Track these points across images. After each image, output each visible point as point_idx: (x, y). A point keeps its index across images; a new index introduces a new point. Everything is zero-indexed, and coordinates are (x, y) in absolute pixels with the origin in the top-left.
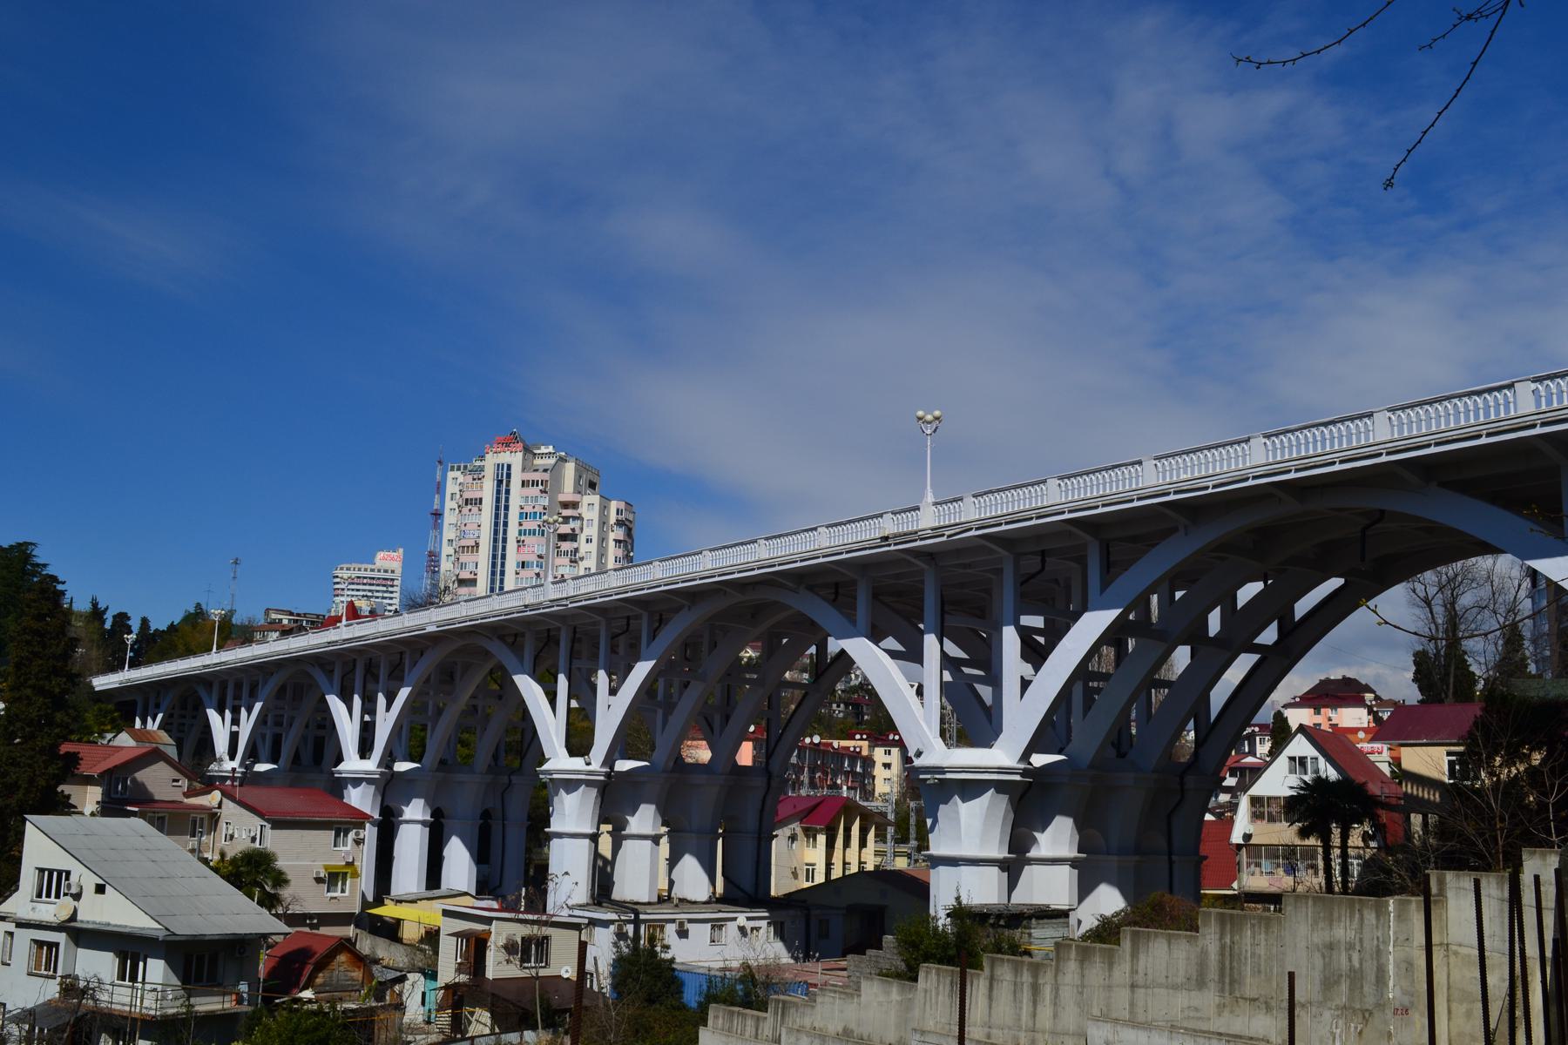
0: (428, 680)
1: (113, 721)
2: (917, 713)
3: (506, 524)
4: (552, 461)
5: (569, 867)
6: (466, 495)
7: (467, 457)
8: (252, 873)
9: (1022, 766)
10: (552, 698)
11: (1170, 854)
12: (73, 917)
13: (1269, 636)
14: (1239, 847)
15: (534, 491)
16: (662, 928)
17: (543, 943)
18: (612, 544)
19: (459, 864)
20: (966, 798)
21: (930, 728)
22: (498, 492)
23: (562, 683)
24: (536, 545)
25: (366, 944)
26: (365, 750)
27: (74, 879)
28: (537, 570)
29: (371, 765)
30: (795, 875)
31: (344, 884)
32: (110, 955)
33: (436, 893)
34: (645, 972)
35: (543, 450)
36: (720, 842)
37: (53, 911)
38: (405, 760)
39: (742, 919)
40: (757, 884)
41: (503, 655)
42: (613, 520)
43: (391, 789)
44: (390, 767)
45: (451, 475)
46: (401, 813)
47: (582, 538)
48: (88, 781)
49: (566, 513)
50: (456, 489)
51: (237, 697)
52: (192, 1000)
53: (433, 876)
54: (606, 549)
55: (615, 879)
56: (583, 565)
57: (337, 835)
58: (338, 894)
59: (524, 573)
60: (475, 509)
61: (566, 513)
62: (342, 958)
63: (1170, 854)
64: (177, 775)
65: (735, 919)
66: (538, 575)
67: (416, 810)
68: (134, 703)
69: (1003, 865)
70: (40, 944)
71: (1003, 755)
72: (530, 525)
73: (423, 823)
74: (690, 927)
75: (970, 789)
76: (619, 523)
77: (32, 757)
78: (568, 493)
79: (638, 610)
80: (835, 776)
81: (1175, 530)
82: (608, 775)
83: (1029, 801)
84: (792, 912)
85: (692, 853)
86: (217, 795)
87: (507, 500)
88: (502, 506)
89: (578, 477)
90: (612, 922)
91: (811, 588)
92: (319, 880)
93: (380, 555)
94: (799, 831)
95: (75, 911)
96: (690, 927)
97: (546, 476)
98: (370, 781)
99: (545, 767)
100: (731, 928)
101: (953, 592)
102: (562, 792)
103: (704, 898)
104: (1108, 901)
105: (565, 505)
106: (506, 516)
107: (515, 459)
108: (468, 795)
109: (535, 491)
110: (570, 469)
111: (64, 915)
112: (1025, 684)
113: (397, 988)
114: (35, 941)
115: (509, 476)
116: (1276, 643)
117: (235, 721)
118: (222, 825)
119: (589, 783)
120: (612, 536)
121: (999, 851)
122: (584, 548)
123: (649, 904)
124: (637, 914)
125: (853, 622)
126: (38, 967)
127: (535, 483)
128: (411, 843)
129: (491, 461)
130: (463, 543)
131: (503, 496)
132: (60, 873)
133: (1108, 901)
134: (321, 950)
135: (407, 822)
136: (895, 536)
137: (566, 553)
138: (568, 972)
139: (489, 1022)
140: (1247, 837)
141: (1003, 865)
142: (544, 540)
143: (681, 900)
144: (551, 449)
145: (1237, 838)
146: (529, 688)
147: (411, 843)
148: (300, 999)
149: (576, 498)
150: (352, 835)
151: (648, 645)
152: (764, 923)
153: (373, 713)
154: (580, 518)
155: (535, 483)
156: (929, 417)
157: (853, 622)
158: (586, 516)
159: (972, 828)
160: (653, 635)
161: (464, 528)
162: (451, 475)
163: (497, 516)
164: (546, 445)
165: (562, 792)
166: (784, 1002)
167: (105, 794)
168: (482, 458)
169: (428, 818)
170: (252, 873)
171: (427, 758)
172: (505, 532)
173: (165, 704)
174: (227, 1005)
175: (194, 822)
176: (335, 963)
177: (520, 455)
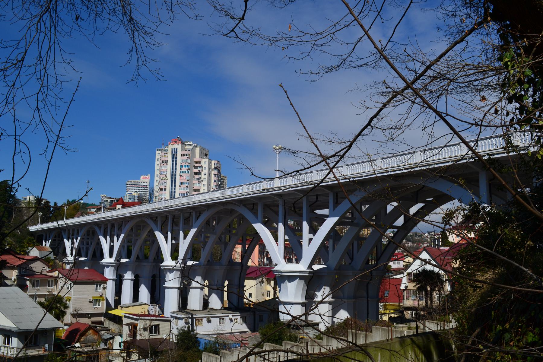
0: (132, 229)
1: (33, 243)
3: (176, 169)
4: (192, 147)
9: (308, 270)
10: (166, 238)
11: (368, 298)
13: (400, 221)
14: (404, 290)
15: (185, 158)
16: (202, 320)
17: (157, 327)
18: (213, 175)
19: (144, 293)
20: (290, 281)
21: (280, 254)
22: (173, 158)
23: (169, 235)
24: (186, 176)
25: (108, 324)
26: (111, 255)
28: (187, 185)
29: (112, 260)
30: (263, 295)
31: (99, 303)
33: (136, 303)
34: (188, 339)
35: (189, 143)
38: (125, 258)
39: (230, 316)
40: (238, 303)
42: (213, 167)
43: (120, 269)
44: (119, 261)
45: (157, 152)
46: (124, 276)
47: (202, 174)
48: (13, 268)
49: (197, 165)
52: (27, 351)
53: (136, 297)
54: (211, 177)
55: (188, 302)
56: (203, 183)
57: (97, 286)
58: (97, 306)
59: (182, 186)
60: (165, 164)
61: (197, 165)
62: (90, 332)
63: (368, 298)
64: (44, 265)
66: (187, 187)
67: (129, 275)
68: (43, 235)
71: (301, 267)
72: (184, 169)
73: (131, 280)
74: (211, 319)
75: (291, 278)
76: (215, 168)
78: (197, 158)
79: (192, 211)
80: (290, 255)
81: (356, 190)
83: (312, 281)
86: (57, 272)
88: (174, 163)
90: (184, 318)
91: (244, 205)
92: (90, 302)
93: (142, 177)
94: (264, 280)
96: (212, 319)
97: (189, 152)
99: (163, 264)
100: (227, 319)
101: (292, 208)
102: (168, 273)
103: (219, 308)
105: (196, 162)
106: (176, 166)
107: (179, 146)
108: (147, 270)
109: (186, 158)
110: (198, 150)
112: (310, 240)
113: (111, 341)
115: (176, 152)
116: (403, 225)
117: (73, 243)
120: (213, 173)
121: (301, 299)
122: (203, 177)
123: (199, 311)
124: (192, 315)
125: (257, 218)
127: (185, 155)
128: (127, 287)
129: (170, 147)
130: (161, 176)
133: (343, 315)
134: (83, 329)
135: (126, 279)
136: (267, 189)
137: (197, 179)
139: (459, 222)
140: (406, 287)
141: (303, 304)
142: (189, 175)
143: (211, 309)
144: (191, 143)
145: (402, 287)
146: (159, 236)
147: (127, 287)
148: (75, 346)
149: (200, 160)
150: (102, 286)
151: (195, 222)
152: (239, 317)
154: (201, 167)
155: (185, 155)
156: (278, 148)
157: (257, 218)
158: (204, 166)
160: (197, 218)
161: (162, 169)
162: (157, 152)
163: (173, 167)
164: (190, 141)
165: (168, 273)
166: (224, 353)
167: (19, 272)
168: (167, 146)
170: (55, 306)
171: (132, 257)
172: (176, 172)
173: (51, 237)
174: (40, 352)
175: (49, 281)
177: (180, 145)
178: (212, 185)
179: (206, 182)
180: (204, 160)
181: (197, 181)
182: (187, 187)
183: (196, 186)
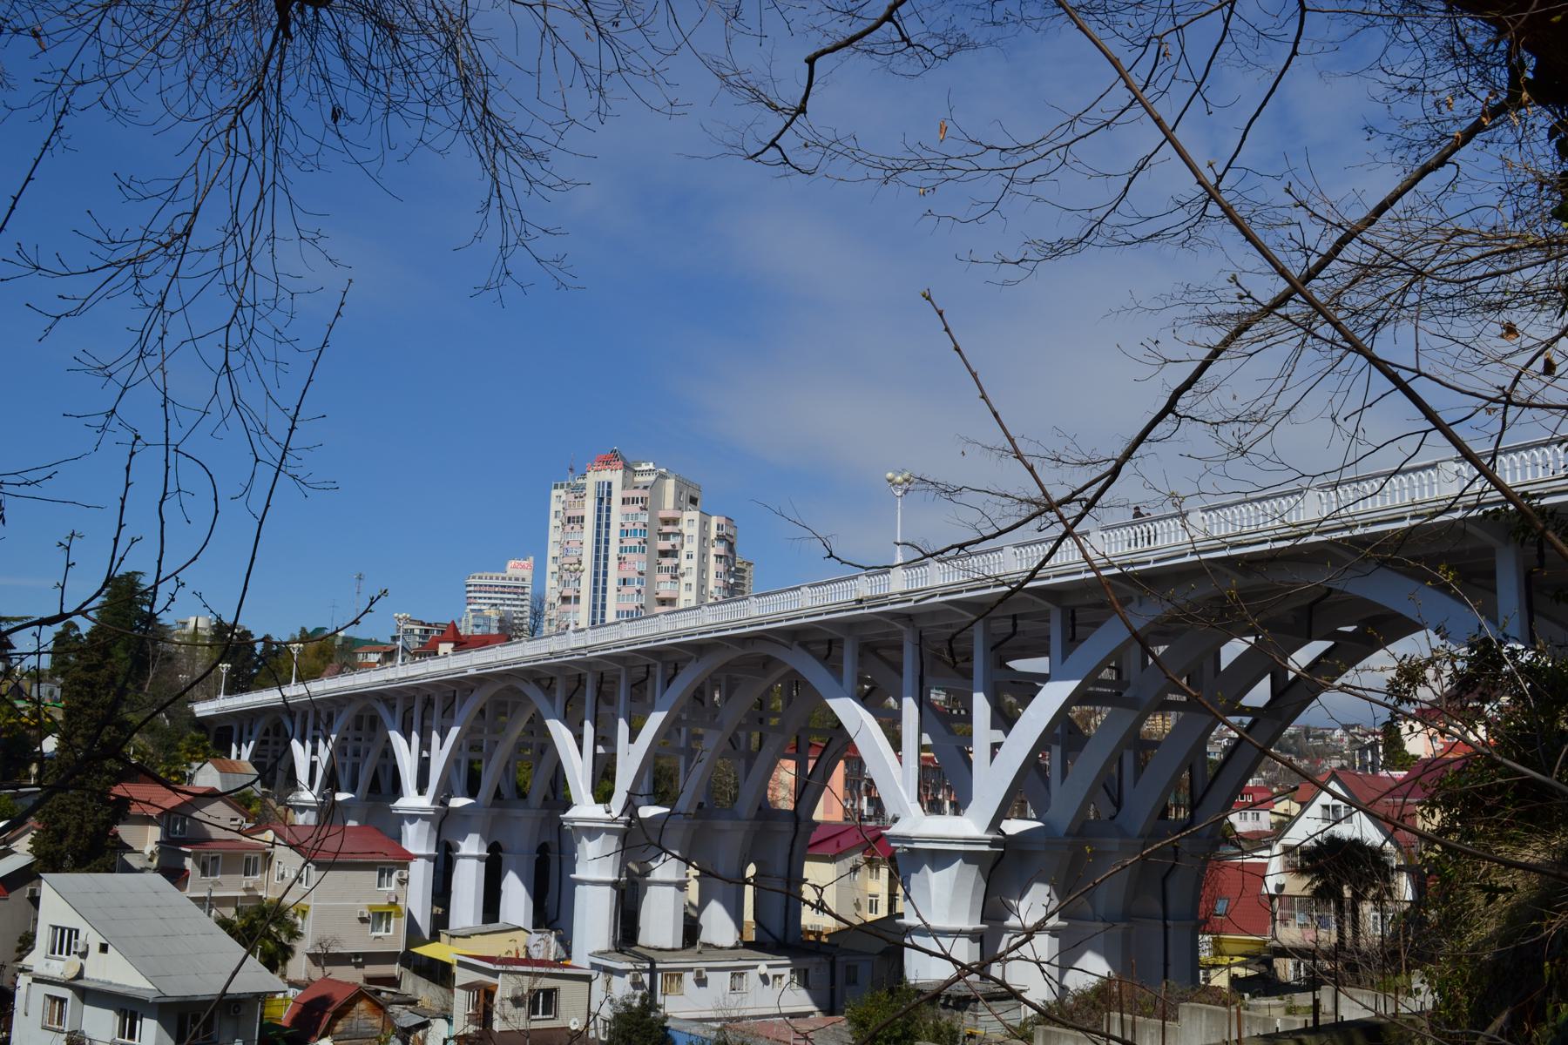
0: (482, 712)
1: (205, 749)
2: (895, 775)
3: (607, 541)
4: (652, 478)
5: (593, 916)
6: (570, 513)
7: (571, 472)
8: (263, 929)
9: (990, 836)
10: (579, 739)
11: (1165, 918)
12: (80, 976)
13: (1260, 694)
14: (1272, 897)
16: (680, 977)
18: (712, 559)
19: (516, 897)
21: (906, 788)
22: (600, 510)
23: (588, 730)
24: (637, 562)
26: (422, 787)
27: (82, 936)
29: (425, 802)
30: (858, 905)
31: (388, 923)
32: (112, 1013)
35: (644, 467)
36: (749, 891)
37: (62, 967)
38: (463, 796)
40: (786, 929)
41: (539, 700)
42: (713, 536)
43: (446, 826)
44: (444, 803)
45: (555, 493)
47: (683, 554)
48: (147, 820)
49: (666, 529)
50: (560, 507)
51: (316, 728)
54: (707, 564)
56: (684, 581)
57: (381, 875)
58: (382, 933)
59: (625, 590)
60: (577, 527)
61: (666, 529)
62: (362, 1005)
63: (1165, 918)
65: (756, 967)
66: (639, 591)
67: (471, 846)
68: (230, 729)
69: (974, 936)
70: (54, 999)
71: (970, 826)
72: (631, 542)
73: (479, 858)
75: (940, 859)
76: (720, 538)
77: (81, 804)
78: (668, 509)
79: (652, 661)
80: (936, 790)
82: (628, 824)
83: (1001, 868)
84: (816, 959)
85: (718, 900)
87: (608, 517)
88: (603, 523)
89: (678, 494)
90: (628, 971)
91: (804, 645)
92: (363, 920)
93: (512, 563)
95: (82, 968)
96: (710, 975)
97: (646, 493)
98: (425, 818)
99: (569, 814)
100: (752, 977)
104: (1093, 968)
105: (666, 522)
106: (607, 533)
107: (615, 476)
109: (635, 508)
110: (670, 486)
111: (72, 972)
112: (996, 746)
113: (420, 1034)
114: (50, 996)
115: (609, 493)
117: (314, 752)
118: (275, 863)
119: (609, 831)
120: (713, 551)
122: (685, 563)
123: (673, 950)
124: (653, 963)
125: (840, 680)
126: (51, 1021)
127: (635, 501)
128: (468, 879)
129: (592, 479)
130: (567, 560)
131: (603, 546)
132: (71, 931)
134: (340, 998)
135: (464, 857)
137: (667, 569)
138: (575, 1024)
140: (1280, 888)
142: (644, 557)
143: (707, 945)
144: (651, 466)
147: (468, 879)
149: (676, 514)
150: (395, 875)
152: (786, 971)
153: (429, 750)
154: (680, 534)
155: (635, 501)
156: (899, 479)
157: (840, 680)
158: (687, 531)
159: (945, 901)
162: (555, 493)
164: (647, 462)
165: (584, 839)
167: (166, 833)
168: (584, 476)
169: (484, 853)
172: (606, 549)
175: (248, 860)
176: (354, 1011)
177: (620, 473)
178: (711, 587)
179: (692, 578)
180: (687, 515)
181: (666, 576)
182: (639, 591)
183: (665, 590)
